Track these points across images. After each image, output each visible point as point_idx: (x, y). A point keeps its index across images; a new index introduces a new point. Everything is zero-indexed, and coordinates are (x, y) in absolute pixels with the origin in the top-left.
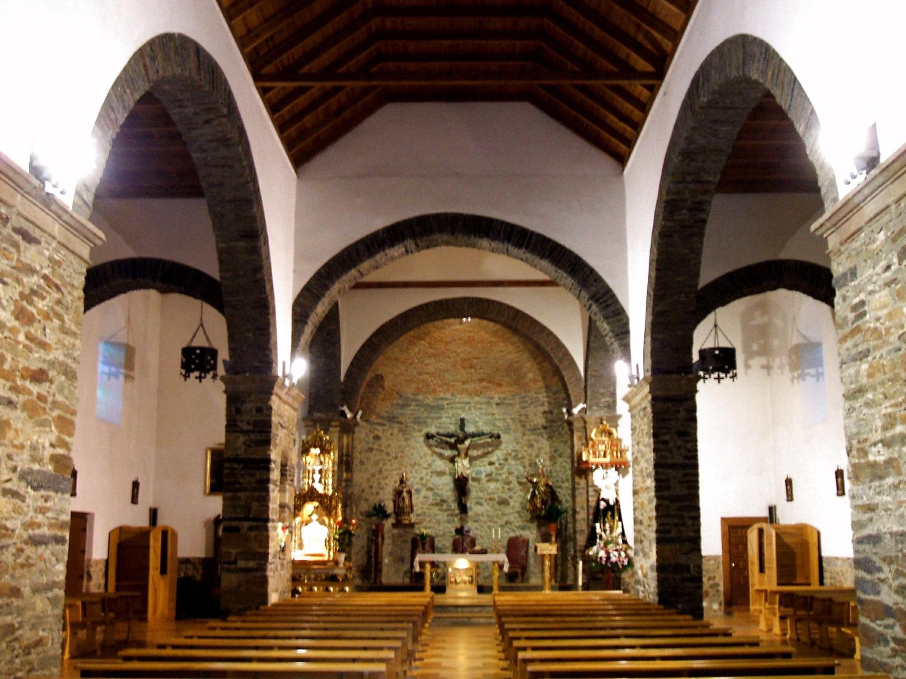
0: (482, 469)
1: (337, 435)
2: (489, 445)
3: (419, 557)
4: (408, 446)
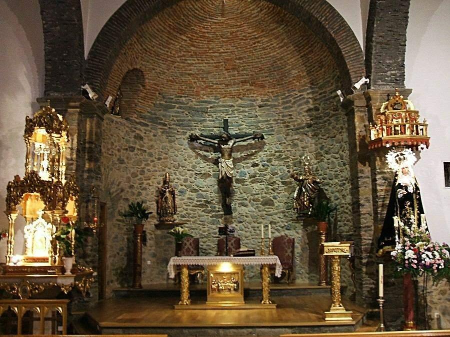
0: (246, 170)
1: (76, 117)
2: (251, 146)
3: (174, 261)
4: (172, 147)
